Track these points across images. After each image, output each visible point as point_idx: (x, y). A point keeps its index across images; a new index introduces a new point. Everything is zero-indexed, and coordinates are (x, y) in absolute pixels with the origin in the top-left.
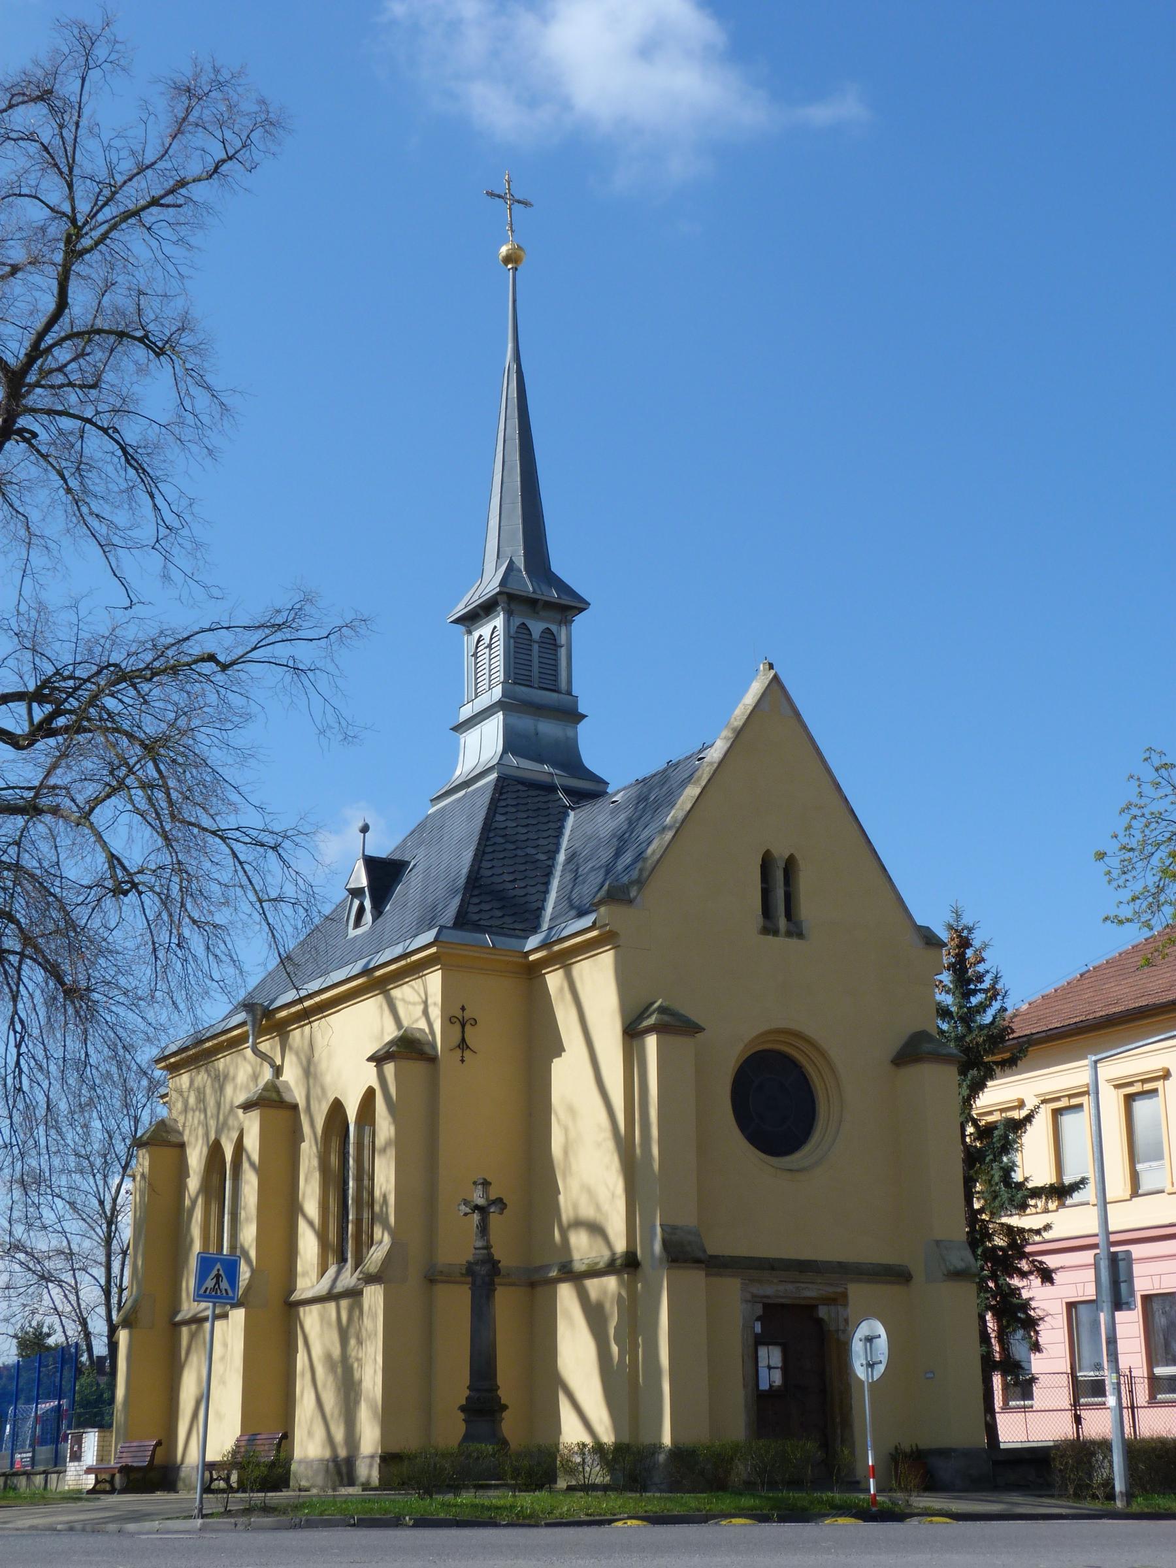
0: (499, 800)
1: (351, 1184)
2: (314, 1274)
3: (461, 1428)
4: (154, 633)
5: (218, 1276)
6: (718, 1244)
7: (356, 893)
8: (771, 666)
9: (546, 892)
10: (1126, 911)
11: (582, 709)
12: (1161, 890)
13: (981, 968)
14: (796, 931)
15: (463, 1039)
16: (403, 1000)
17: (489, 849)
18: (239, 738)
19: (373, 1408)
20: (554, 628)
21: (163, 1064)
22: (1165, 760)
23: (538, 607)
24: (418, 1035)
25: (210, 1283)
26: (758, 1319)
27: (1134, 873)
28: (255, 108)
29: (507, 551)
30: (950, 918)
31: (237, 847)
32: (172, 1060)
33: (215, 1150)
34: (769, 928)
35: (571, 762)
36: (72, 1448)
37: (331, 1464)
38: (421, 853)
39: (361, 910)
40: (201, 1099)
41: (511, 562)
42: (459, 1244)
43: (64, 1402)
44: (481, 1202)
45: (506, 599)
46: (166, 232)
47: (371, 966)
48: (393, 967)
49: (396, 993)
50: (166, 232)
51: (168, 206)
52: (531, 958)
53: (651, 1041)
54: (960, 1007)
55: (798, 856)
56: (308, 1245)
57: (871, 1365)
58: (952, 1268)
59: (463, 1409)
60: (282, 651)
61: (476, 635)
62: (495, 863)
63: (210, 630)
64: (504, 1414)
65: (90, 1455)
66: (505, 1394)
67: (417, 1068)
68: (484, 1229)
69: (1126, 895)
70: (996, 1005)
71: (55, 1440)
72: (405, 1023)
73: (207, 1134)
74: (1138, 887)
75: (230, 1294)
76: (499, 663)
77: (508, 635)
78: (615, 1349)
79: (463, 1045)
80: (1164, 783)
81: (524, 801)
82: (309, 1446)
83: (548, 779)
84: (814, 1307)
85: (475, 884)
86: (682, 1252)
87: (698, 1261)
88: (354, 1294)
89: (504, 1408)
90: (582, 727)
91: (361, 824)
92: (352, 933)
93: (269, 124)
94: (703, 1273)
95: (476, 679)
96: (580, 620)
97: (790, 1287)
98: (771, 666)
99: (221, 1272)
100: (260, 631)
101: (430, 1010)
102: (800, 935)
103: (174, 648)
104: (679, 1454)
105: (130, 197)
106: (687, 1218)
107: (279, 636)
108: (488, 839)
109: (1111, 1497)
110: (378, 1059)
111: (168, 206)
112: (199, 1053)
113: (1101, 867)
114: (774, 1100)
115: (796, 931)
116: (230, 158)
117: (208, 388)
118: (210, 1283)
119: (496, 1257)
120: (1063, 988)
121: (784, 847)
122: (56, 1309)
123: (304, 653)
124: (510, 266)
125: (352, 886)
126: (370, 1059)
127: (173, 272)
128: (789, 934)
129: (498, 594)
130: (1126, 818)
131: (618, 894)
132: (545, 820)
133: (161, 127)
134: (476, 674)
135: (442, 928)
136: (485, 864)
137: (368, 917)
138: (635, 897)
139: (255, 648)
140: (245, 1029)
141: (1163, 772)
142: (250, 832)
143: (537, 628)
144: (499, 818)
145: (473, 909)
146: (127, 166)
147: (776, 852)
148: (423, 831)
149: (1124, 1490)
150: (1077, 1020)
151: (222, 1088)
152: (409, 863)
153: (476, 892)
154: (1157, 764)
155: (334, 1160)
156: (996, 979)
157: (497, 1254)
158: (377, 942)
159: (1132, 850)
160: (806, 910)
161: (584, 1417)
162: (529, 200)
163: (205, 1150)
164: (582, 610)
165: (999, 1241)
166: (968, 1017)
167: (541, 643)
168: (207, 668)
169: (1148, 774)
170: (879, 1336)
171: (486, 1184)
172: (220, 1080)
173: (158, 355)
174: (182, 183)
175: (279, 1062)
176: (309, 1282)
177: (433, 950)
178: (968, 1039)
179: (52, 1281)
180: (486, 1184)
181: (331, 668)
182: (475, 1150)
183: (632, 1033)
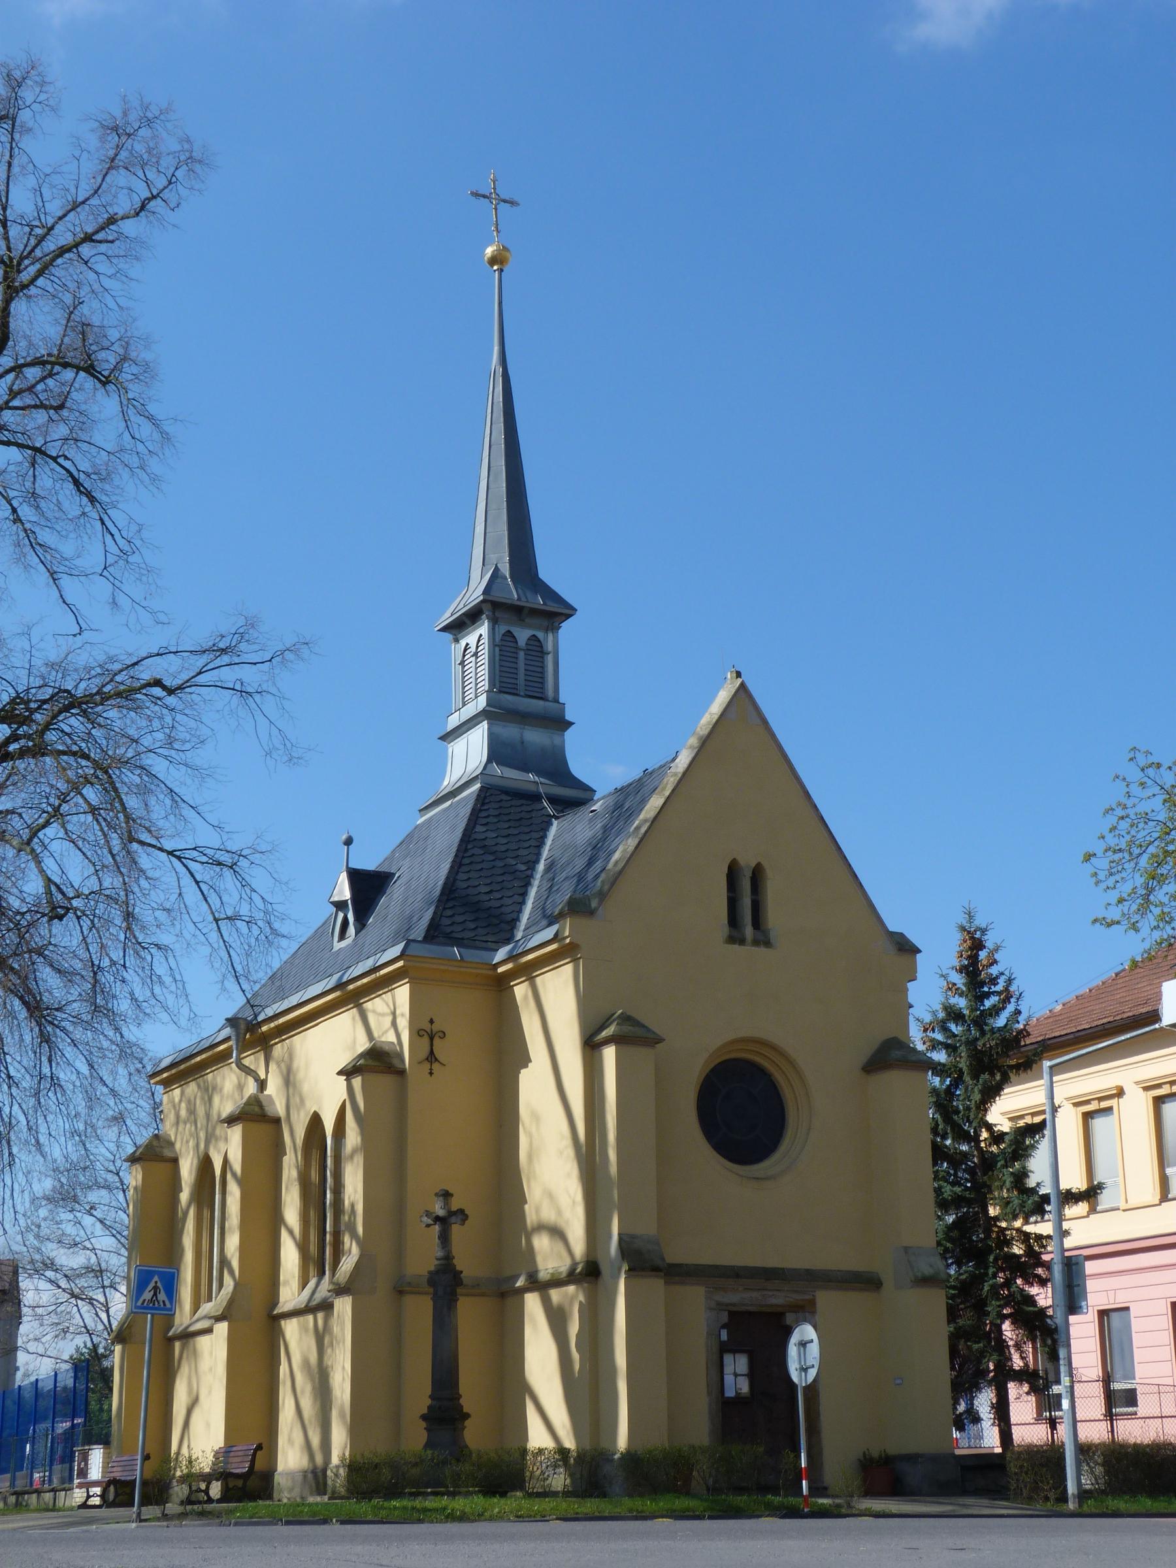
0: (481, 810)
1: (328, 1196)
2: (295, 1284)
3: (423, 1437)
4: (102, 658)
5: (155, 1288)
6: (675, 1254)
7: (340, 906)
8: (739, 674)
9: (523, 903)
10: (1114, 913)
11: (569, 717)
12: (1150, 891)
13: (994, 971)
14: (763, 940)
15: (432, 1052)
16: (374, 1011)
17: (466, 861)
18: (200, 757)
19: (342, 1415)
20: (540, 635)
21: (158, 1079)
22: (1151, 759)
23: (523, 614)
24: (387, 1048)
25: (147, 1295)
26: (723, 1327)
27: (1124, 874)
28: (176, 147)
29: (493, 558)
30: (962, 920)
31: (191, 864)
32: (165, 1075)
33: (205, 1164)
34: (735, 936)
35: (557, 769)
36: (79, 1465)
37: (310, 1476)
38: (406, 863)
39: (345, 923)
40: (192, 1111)
41: (497, 569)
42: (423, 1256)
43: (78, 1421)
44: (441, 1213)
45: (491, 607)
46: (102, 266)
47: (345, 979)
48: (365, 981)
49: (368, 1006)
50: (102, 266)
51: (100, 242)
52: (500, 970)
53: (609, 1054)
54: (973, 1010)
55: (765, 864)
56: (290, 1256)
57: (804, 1370)
58: (919, 1275)
59: (424, 1417)
60: (228, 675)
61: (463, 643)
62: (472, 874)
63: (158, 655)
64: (467, 1423)
65: (95, 1471)
66: (468, 1403)
67: (385, 1082)
68: (445, 1238)
69: (1113, 896)
70: (1011, 1008)
71: (67, 1457)
72: (376, 1035)
73: (197, 1145)
74: (1126, 888)
75: (168, 1305)
76: (484, 671)
77: (493, 644)
78: (576, 1356)
79: (431, 1057)
80: (1150, 782)
81: (507, 811)
82: (290, 1458)
83: (532, 788)
84: (781, 1315)
85: (450, 895)
86: (641, 1259)
87: (656, 1269)
88: (326, 1307)
89: (467, 1416)
90: (569, 734)
91: (344, 837)
92: (338, 946)
93: (191, 160)
94: (662, 1281)
95: (464, 688)
96: (567, 628)
97: (755, 1294)
98: (739, 674)
99: (159, 1284)
100: (205, 656)
101: (398, 1020)
102: (767, 944)
103: (124, 673)
104: (630, 1457)
105: (62, 236)
106: (647, 1227)
107: (226, 659)
108: (466, 850)
109: (1063, 1498)
110: (348, 1073)
111: (100, 242)
112: (187, 1069)
113: (1088, 868)
114: (742, 1109)
115: (763, 940)
116: (154, 197)
117: (150, 418)
118: (147, 1295)
119: (458, 1268)
120: (1098, 988)
121: (753, 859)
122: (86, 1327)
123: (250, 676)
124: (495, 267)
125: (336, 898)
126: (340, 1073)
127: (112, 304)
128: (756, 943)
129: (482, 602)
130: (1112, 820)
131: (578, 907)
132: (527, 830)
133: (90, 166)
134: (463, 682)
135: (409, 942)
136: (461, 876)
137: (351, 930)
138: (596, 909)
139: (200, 673)
140: (230, 1043)
141: (1151, 772)
142: (208, 851)
143: (523, 635)
144: (479, 828)
145: (447, 922)
146: (55, 208)
147: (742, 862)
148: (412, 841)
149: (1076, 1492)
150: (1105, 1021)
151: (210, 1099)
152: (394, 874)
153: (450, 904)
154: (1142, 763)
155: (314, 1176)
156: (1010, 981)
157: (459, 1264)
158: (357, 953)
159: (1120, 850)
160: (774, 917)
161: (549, 1424)
162: (516, 199)
163: (195, 1162)
164: (569, 616)
165: (1018, 1249)
166: (980, 1021)
167: (527, 651)
168: (157, 691)
169: (1134, 774)
170: (812, 1341)
171: (446, 1195)
172: (209, 1093)
173: (104, 384)
174: (112, 221)
175: (263, 1076)
176: (290, 1295)
177: (401, 963)
178: (980, 1043)
179: (82, 1299)
180: (446, 1195)
181: (273, 690)
182: (443, 1159)
183: (591, 1046)
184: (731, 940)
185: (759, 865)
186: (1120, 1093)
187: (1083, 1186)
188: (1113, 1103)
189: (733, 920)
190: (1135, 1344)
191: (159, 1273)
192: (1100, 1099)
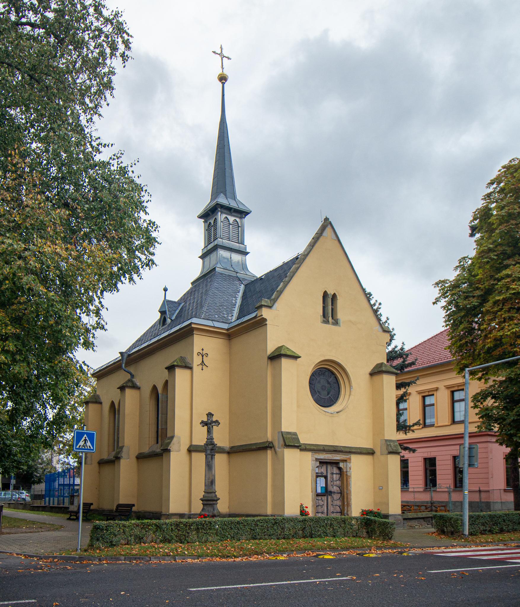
5: (85, 440)
14: (336, 322)
15: (203, 361)
20: (238, 220)
55: (337, 294)
99: (87, 438)
115: (336, 322)
126: (166, 368)
128: (333, 324)
157: (216, 441)
160: (340, 315)
185: (335, 294)
186: (437, 389)
187: (194, 454)
189: (324, 315)
190: (437, 474)
191: (87, 434)
192: (429, 391)
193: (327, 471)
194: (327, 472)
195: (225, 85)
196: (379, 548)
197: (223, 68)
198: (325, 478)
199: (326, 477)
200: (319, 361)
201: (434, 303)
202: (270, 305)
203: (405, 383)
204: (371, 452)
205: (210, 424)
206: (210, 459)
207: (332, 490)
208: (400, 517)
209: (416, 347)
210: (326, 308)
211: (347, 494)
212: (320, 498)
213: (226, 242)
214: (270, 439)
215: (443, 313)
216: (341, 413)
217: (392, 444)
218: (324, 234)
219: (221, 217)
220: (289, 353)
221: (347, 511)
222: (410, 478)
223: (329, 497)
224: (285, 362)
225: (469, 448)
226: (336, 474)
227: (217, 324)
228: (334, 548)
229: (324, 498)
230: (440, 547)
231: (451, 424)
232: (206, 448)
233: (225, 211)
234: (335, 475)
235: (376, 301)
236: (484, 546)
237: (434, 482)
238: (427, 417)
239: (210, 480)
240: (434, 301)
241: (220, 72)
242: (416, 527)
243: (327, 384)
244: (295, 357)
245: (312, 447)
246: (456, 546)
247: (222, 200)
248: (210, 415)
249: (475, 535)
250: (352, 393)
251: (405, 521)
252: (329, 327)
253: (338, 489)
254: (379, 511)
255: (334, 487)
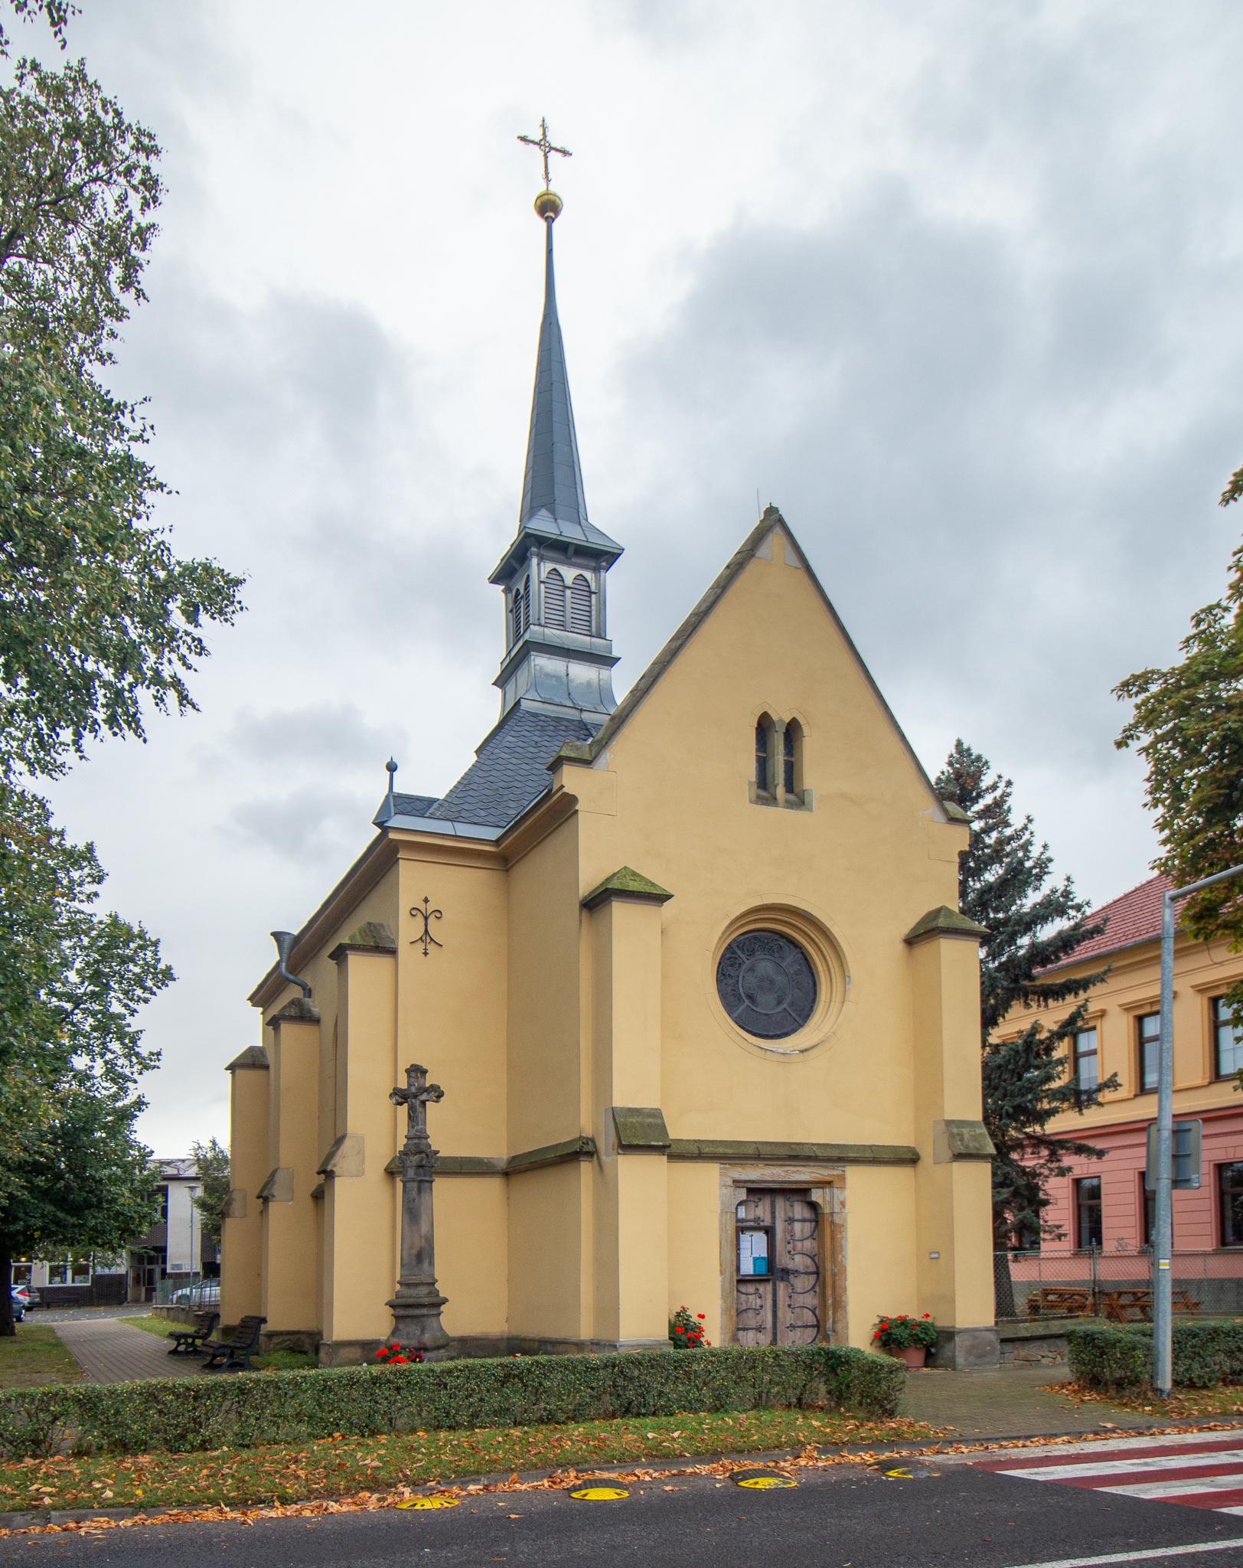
14: (798, 799)
15: (426, 931)
115: (798, 799)
128: (789, 805)
160: (811, 779)
184: (760, 800)
188: (1098, 1024)
189: (763, 781)
192: (1152, 1003)
193: (773, 1213)
194: (773, 1217)
195: (555, 225)
196: (830, 1446)
197: (548, 179)
198: (767, 1233)
199: (770, 1232)
200: (744, 909)
201: (1120, 744)
202: (587, 757)
203: (1075, 981)
204: (908, 1158)
205: (416, 1096)
206: (414, 1193)
207: (790, 1266)
208: (991, 1336)
209: (1126, 896)
210: (769, 764)
211: (834, 1275)
212: (751, 1288)
213: (553, 635)
214: (588, 1132)
215: (1146, 767)
216: (815, 1051)
217: (965, 1131)
218: (763, 551)
219: (539, 569)
220: (633, 886)
221: (834, 1322)
222: (1106, 1223)
223: (781, 1287)
224: (620, 911)
225: (1175, 1132)
226: (803, 1220)
227: (463, 830)
228: (666, 1456)
229: (766, 1289)
230: (1056, 1436)
231: (1210, 1083)
232: (402, 1162)
233: (551, 554)
234: (797, 1226)
235: (1000, 777)
236: (1210, 1429)
237: (1096, 1233)
238: (1147, 1070)
239: (414, 1252)
240: (1119, 737)
241: (543, 189)
242: (1044, 1361)
243: (771, 973)
244: (660, 898)
245: (721, 1150)
246: (1113, 1430)
247: (543, 525)
248: (416, 1071)
249: (1205, 1387)
250: (851, 996)
251: (1008, 1347)
252: (778, 815)
253: (809, 1261)
254: (929, 1320)
255: (798, 1258)
